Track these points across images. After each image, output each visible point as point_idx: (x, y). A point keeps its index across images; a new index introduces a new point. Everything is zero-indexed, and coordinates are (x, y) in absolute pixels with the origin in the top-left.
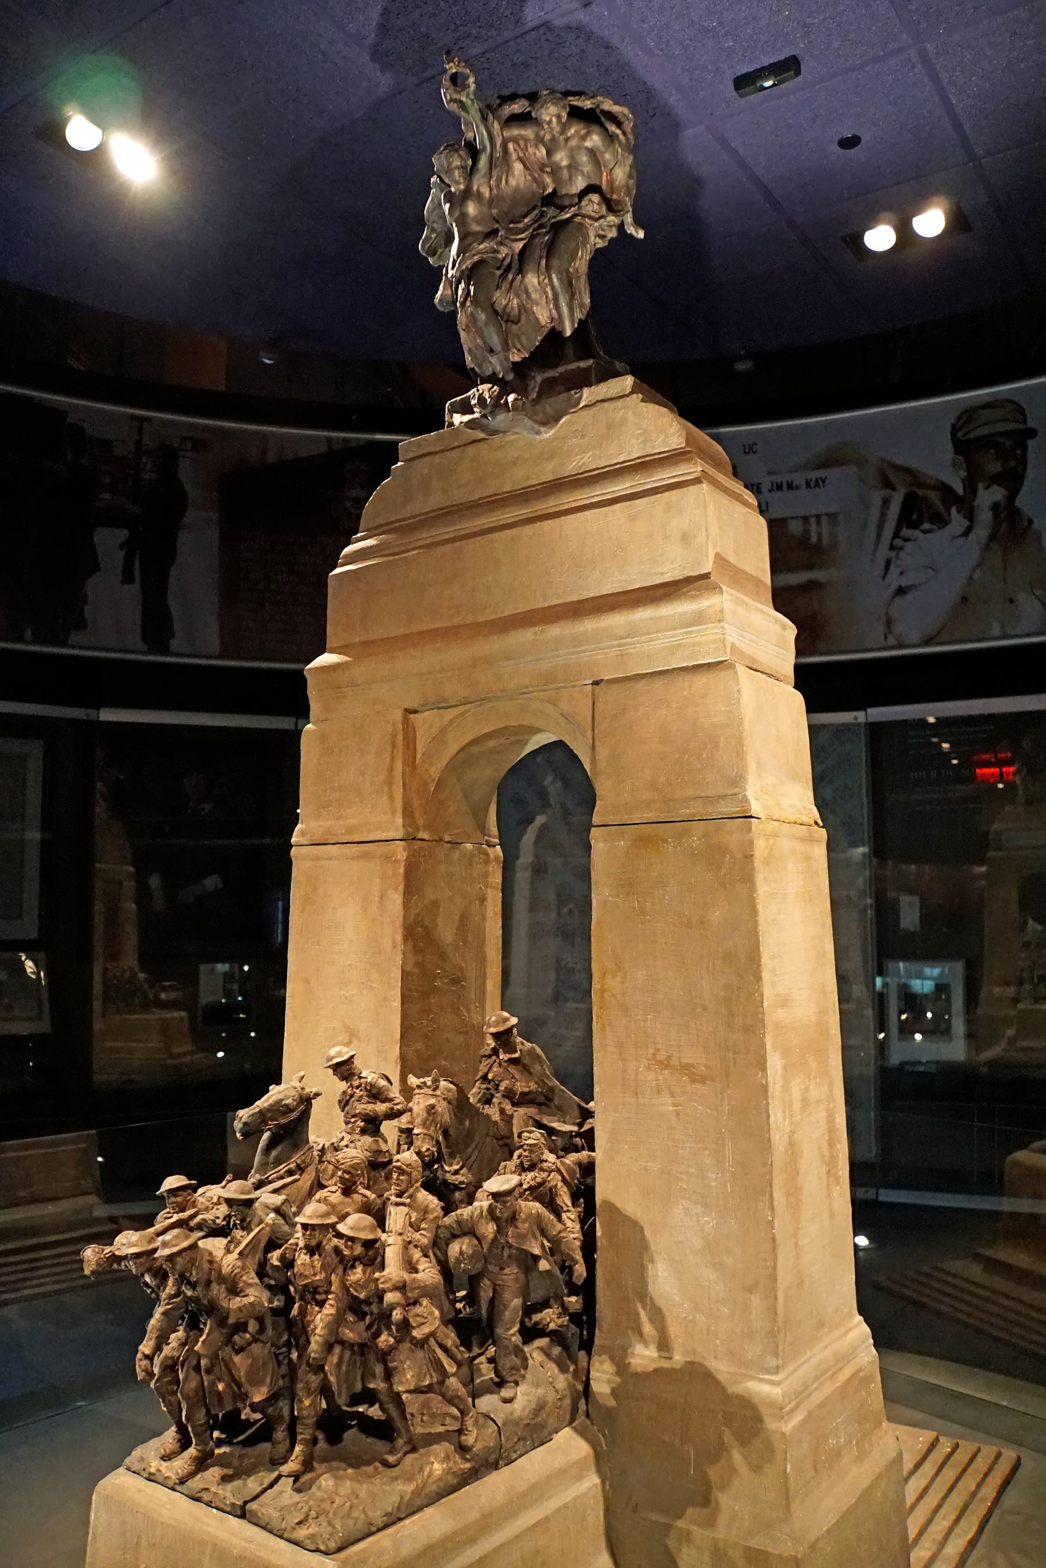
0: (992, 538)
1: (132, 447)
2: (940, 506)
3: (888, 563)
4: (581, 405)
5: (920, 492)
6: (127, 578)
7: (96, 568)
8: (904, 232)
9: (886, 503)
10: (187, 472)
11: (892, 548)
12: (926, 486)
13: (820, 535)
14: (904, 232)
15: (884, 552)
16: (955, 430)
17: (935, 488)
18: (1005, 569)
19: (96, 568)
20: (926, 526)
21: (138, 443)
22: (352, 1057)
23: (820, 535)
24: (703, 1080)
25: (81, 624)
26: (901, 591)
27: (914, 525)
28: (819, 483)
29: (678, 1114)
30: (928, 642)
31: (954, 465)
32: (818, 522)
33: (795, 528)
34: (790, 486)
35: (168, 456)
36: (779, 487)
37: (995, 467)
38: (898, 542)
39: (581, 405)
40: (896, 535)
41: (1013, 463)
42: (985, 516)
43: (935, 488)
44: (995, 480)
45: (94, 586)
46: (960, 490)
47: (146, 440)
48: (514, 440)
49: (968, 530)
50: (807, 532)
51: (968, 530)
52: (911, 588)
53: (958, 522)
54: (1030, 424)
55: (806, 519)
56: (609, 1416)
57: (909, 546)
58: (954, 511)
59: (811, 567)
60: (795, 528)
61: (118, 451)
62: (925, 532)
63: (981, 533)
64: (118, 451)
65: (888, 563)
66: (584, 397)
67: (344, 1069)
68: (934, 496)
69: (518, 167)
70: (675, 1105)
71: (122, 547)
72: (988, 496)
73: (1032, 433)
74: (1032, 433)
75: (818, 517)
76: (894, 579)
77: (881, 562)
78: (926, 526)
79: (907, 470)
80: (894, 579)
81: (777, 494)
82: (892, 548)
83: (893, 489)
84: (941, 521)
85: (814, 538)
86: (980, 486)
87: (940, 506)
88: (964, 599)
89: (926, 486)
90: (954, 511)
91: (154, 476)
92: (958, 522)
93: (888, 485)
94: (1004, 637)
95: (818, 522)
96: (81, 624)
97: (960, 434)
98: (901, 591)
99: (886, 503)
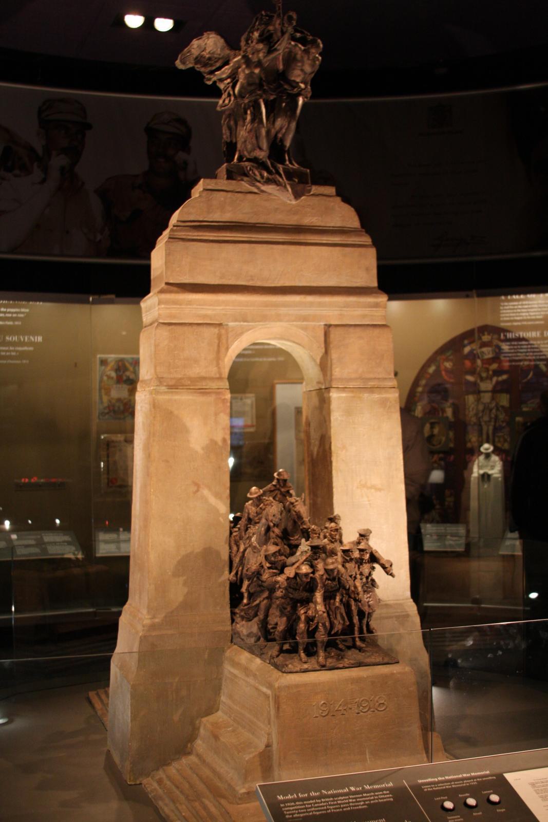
4: (312, 193)
8: (149, 24)
14: (149, 24)
16: (40, 112)
20: (17, 172)
24: (380, 490)
29: (370, 504)
39: (312, 193)
46: (40, 152)
48: (275, 199)
49: (44, 181)
51: (44, 181)
58: (35, 164)
62: (16, 176)
66: (313, 190)
70: (369, 501)
72: (58, 161)
73: (89, 127)
74: (89, 127)
78: (17, 172)
94: (63, 256)
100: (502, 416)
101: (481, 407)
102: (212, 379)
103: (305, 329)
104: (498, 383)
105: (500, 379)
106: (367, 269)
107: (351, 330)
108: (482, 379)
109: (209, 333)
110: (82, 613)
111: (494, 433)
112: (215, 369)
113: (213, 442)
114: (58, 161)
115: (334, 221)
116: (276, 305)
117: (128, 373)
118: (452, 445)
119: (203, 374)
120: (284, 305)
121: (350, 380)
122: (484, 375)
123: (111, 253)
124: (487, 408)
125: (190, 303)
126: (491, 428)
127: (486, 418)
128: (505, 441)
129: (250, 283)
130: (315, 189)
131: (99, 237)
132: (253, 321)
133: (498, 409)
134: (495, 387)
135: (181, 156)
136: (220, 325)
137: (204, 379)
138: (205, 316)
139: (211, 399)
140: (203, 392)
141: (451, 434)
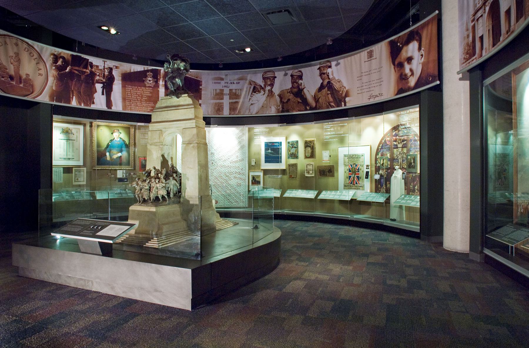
0: (268, 96)
1: (103, 67)
2: (259, 89)
3: (250, 99)
5: (256, 86)
6: (103, 94)
7: (96, 92)
9: (250, 88)
10: (114, 73)
11: (251, 96)
12: (257, 85)
13: (238, 93)
15: (249, 97)
17: (259, 86)
18: (80, 181)
19: (96, 92)
20: (257, 93)
21: (104, 66)
22: (135, 224)
23: (238, 93)
25: (93, 103)
26: (252, 104)
27: (255, 92)
28: (239, 83)
30: (256, 114)
31: (262, 82)
32: (238, 90)
33: (234, 91)
34: (233, 83)
35: (111, 69)
36: (232, 83)
37: (269, 83)
38: (252, 95)
40: (252, 94)
41: (272, 82)
42: (267, 92)
43: (259, 86)
44: (269, 85)
45: (95, 95)
46: (263, 86)
47: (106, 66)
49: (264, 94)
50: (236, 92)
51: (264, 94)
52: (253, 104)
53: (262, 92)
54: (275, 76)
55: (236, 90)
56: (182, 203)
57: (254, 96)
58: (262, 90)
59: (236, 99)
60: (234, 91)
61: (100, 68)
63: (266, 95)
64: (100, 68)
65: (250, 99)
67: (155, 168)
68: (258, 87)
69: (176, 65)
71: (101, 88)
72: (268, 88)
73: (276, 77)
74: (276, 77)
75: (238, 89)
76: (251, 102)
77: (248, 99)
78: (257, 93)
79: (254, 82)
80: (251, 102)
81: (231, 84)
82: (251, 96)
83: (252, 85)
84: (259, 92)
85: (237, 93)
86: (267, 86)
87: (259, 89)
88: (263, 107)
89: (257, 85)
90: (262, 90)
91: (108, 73)
92: (262, 92)
93: (251, 84)
95: (238, 90)
96: (93, 103)
97: (264, 76)
98: (252, 104)
99: (250, 88)
100: (404, 156)
101: (398, 153)
102: (158, 143)
103: (178, 130)
104: (403, 144)
105: (404, 143)
106: (192, 114)
107: (187, 129)
108: (399, 143)
109: (158, 132)
110: (402, 226)
111: (402, 162)
112: (159, 140)
113: (158, 157)
114: (268, 88)
115: (187, 103)
116: (171, 125)
117: (295, 145)
118: (389, 167)
119: (157, 142)
120: (173, 124)
121: (186, 141)
122: (399, 142)
123: (282, 112)
124: (400, 154)
125: (155, 126)
126: (401, 160)
127: (400, 157)
128: (405, 165)
129: (167, 120)
130: (183, 95)
131: (279, 108)
132: (167, 129)
133: (403, 154)
134: (402, 146)
135: (300, 81)
136: (161, 130)
137: (156, 142)
138: (158, 128)
139: (158, 147)
140: (156, 145)
141: (389, 163)
